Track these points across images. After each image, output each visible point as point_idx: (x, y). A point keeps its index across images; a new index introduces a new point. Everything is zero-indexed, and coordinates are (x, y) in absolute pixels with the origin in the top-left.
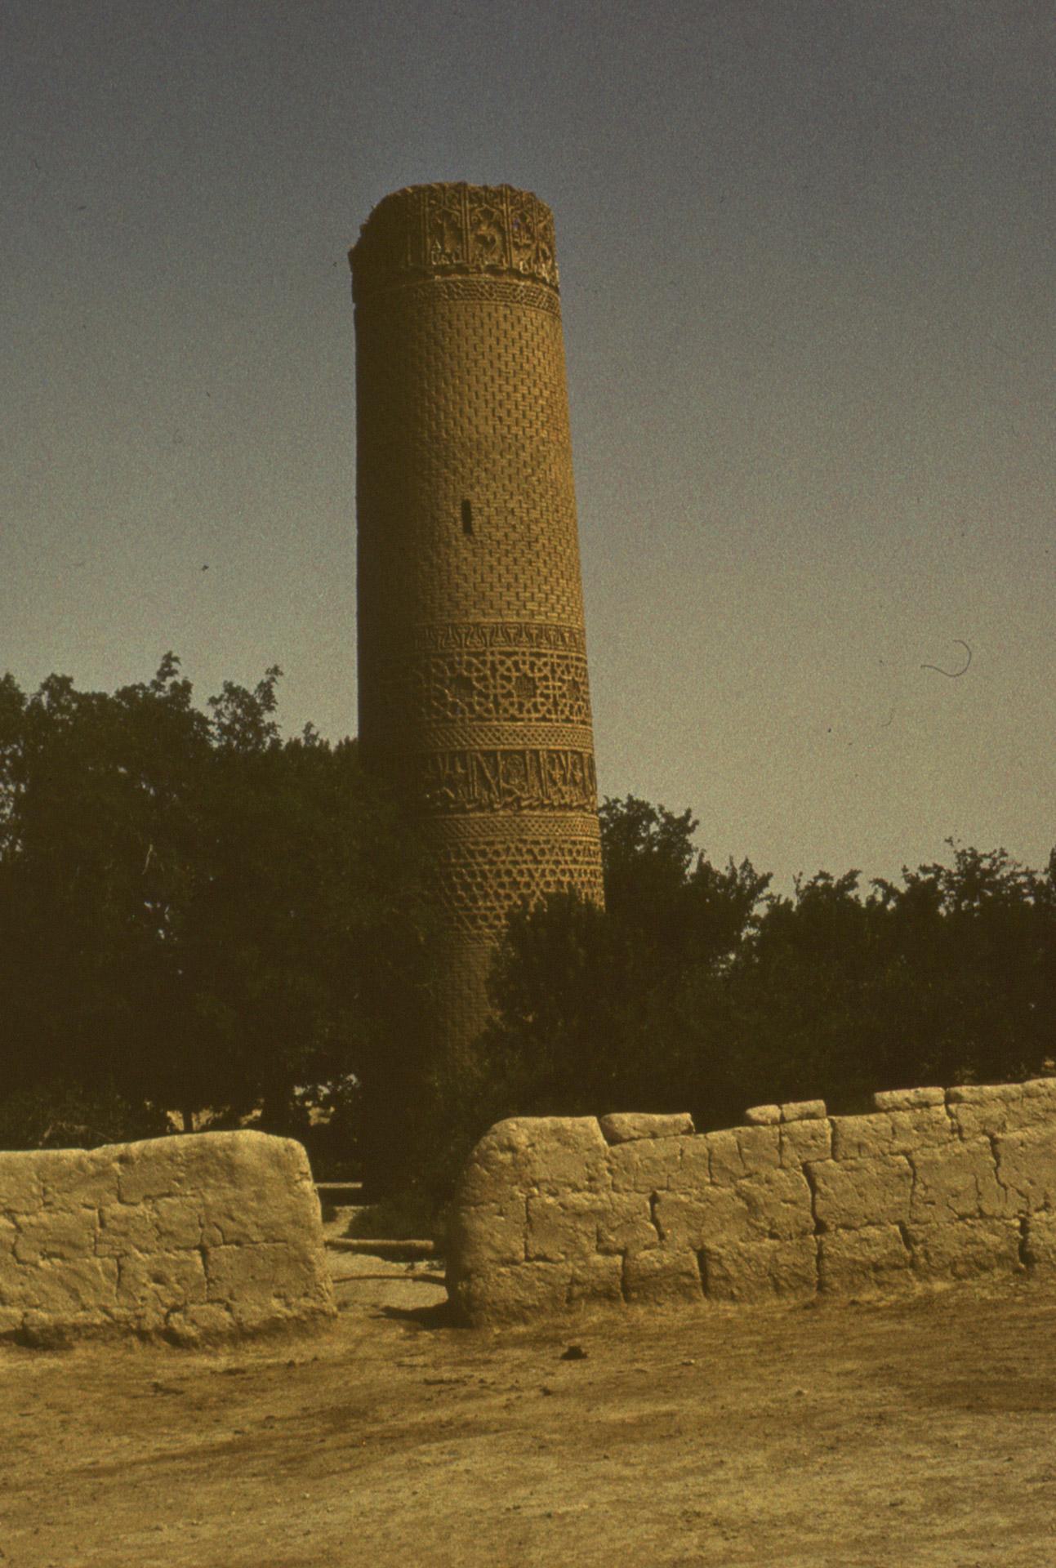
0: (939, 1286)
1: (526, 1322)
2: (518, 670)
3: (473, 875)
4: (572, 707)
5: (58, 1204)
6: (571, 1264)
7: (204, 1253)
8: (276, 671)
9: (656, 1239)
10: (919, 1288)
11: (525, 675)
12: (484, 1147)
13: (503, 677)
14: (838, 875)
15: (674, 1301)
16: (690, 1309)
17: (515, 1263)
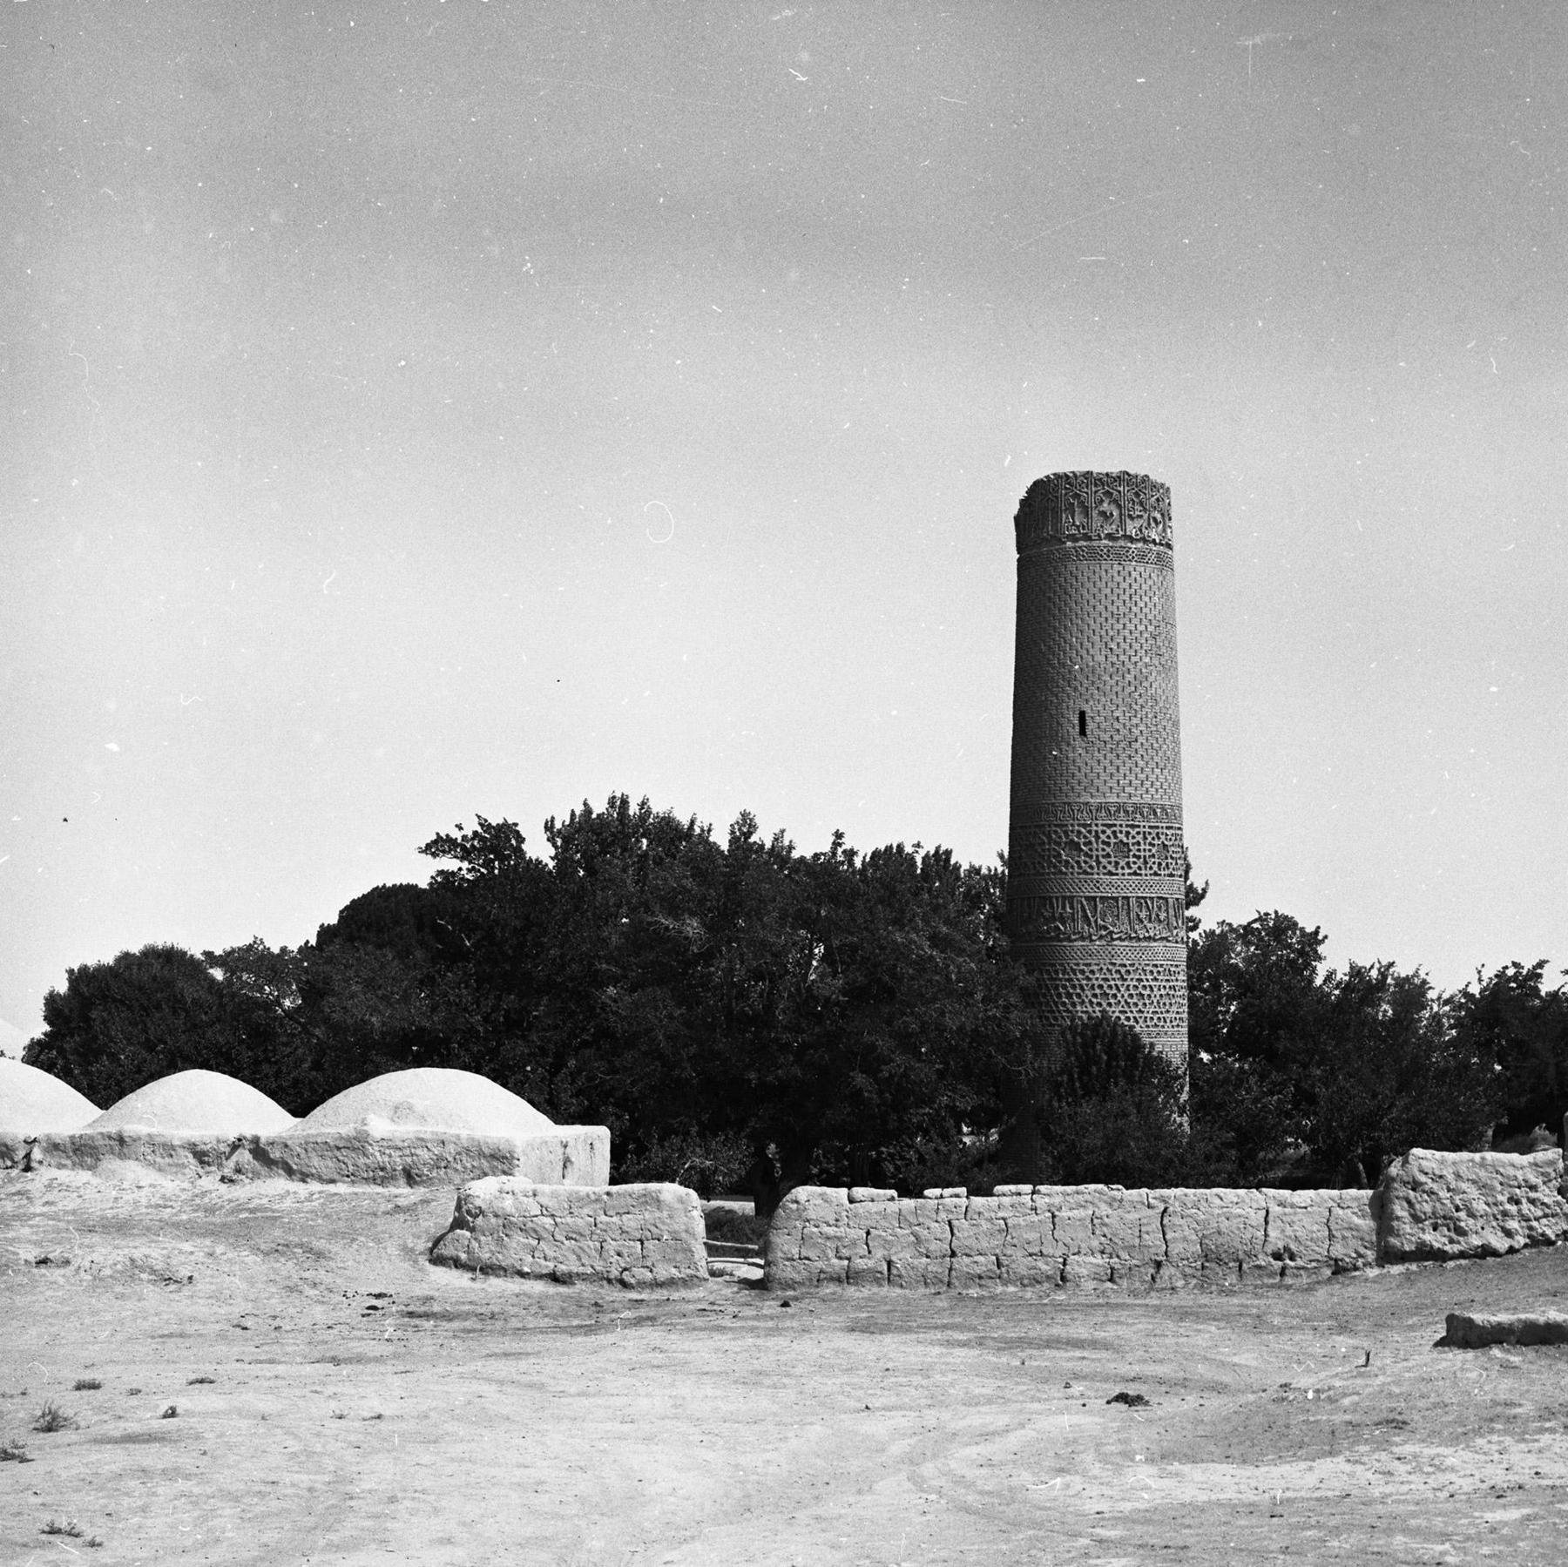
0: (1011, 1289)
3: (1074, 987)
10: (999, 1289)
13: (1104, 843)
14: (1528, 965)
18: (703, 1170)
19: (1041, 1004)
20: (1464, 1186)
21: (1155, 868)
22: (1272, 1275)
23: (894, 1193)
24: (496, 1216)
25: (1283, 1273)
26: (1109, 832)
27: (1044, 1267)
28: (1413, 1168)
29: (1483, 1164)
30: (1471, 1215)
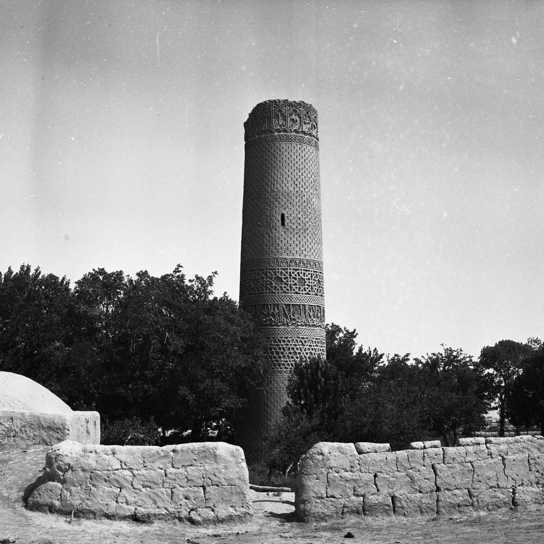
0: (482, 513)
1: (326, 521)
2: (299, 275)
3: (280, 349)
4: (318, 290)
5: (149, 467)
6: (343, 499)
7: (204, 489)
8: (216, 273)
9: (376, 491)
10: (475, 514)
11: (301, 277)
12: (312, 453)
13: (293, 278)
14: (402, 355)
15: (383, 516)
16: (388, 519)
17: (322, 498)
24: (84, 470)
26: (296, 273)
27: (501, 496)
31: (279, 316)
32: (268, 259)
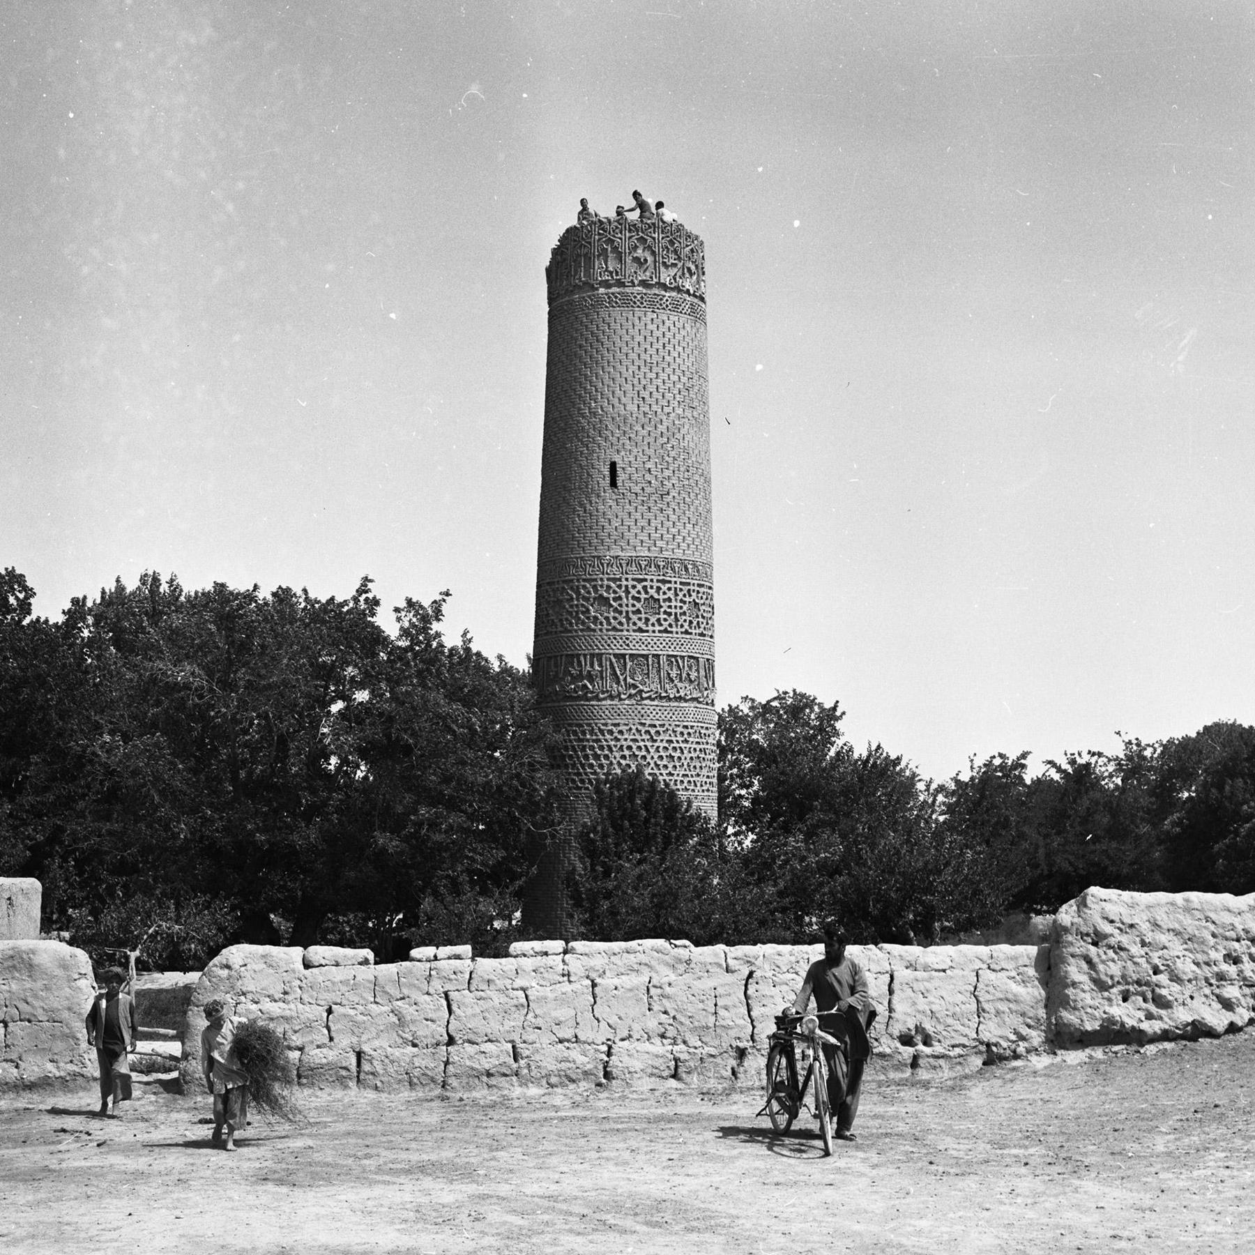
0: (533, 1091)
2: (647, 593)
3: (602, 748)
4: (691, 622)
9: (326, 1040)
10: (518, 1091)
13: (634, 598)
14: (1012, 756)
18: (170, 936)
19: (567, 766)
20: (1163, 938)
21: (686, 625)
22: (899, 1066)
23: (368, 953)
25: (914, 1064)
26: (639, 587)
27: (581, 1059)
28: (1094, 914)
29: (1188, 910)
30: (1175, 978)
31: (602, 678)
32: (582, 558)
